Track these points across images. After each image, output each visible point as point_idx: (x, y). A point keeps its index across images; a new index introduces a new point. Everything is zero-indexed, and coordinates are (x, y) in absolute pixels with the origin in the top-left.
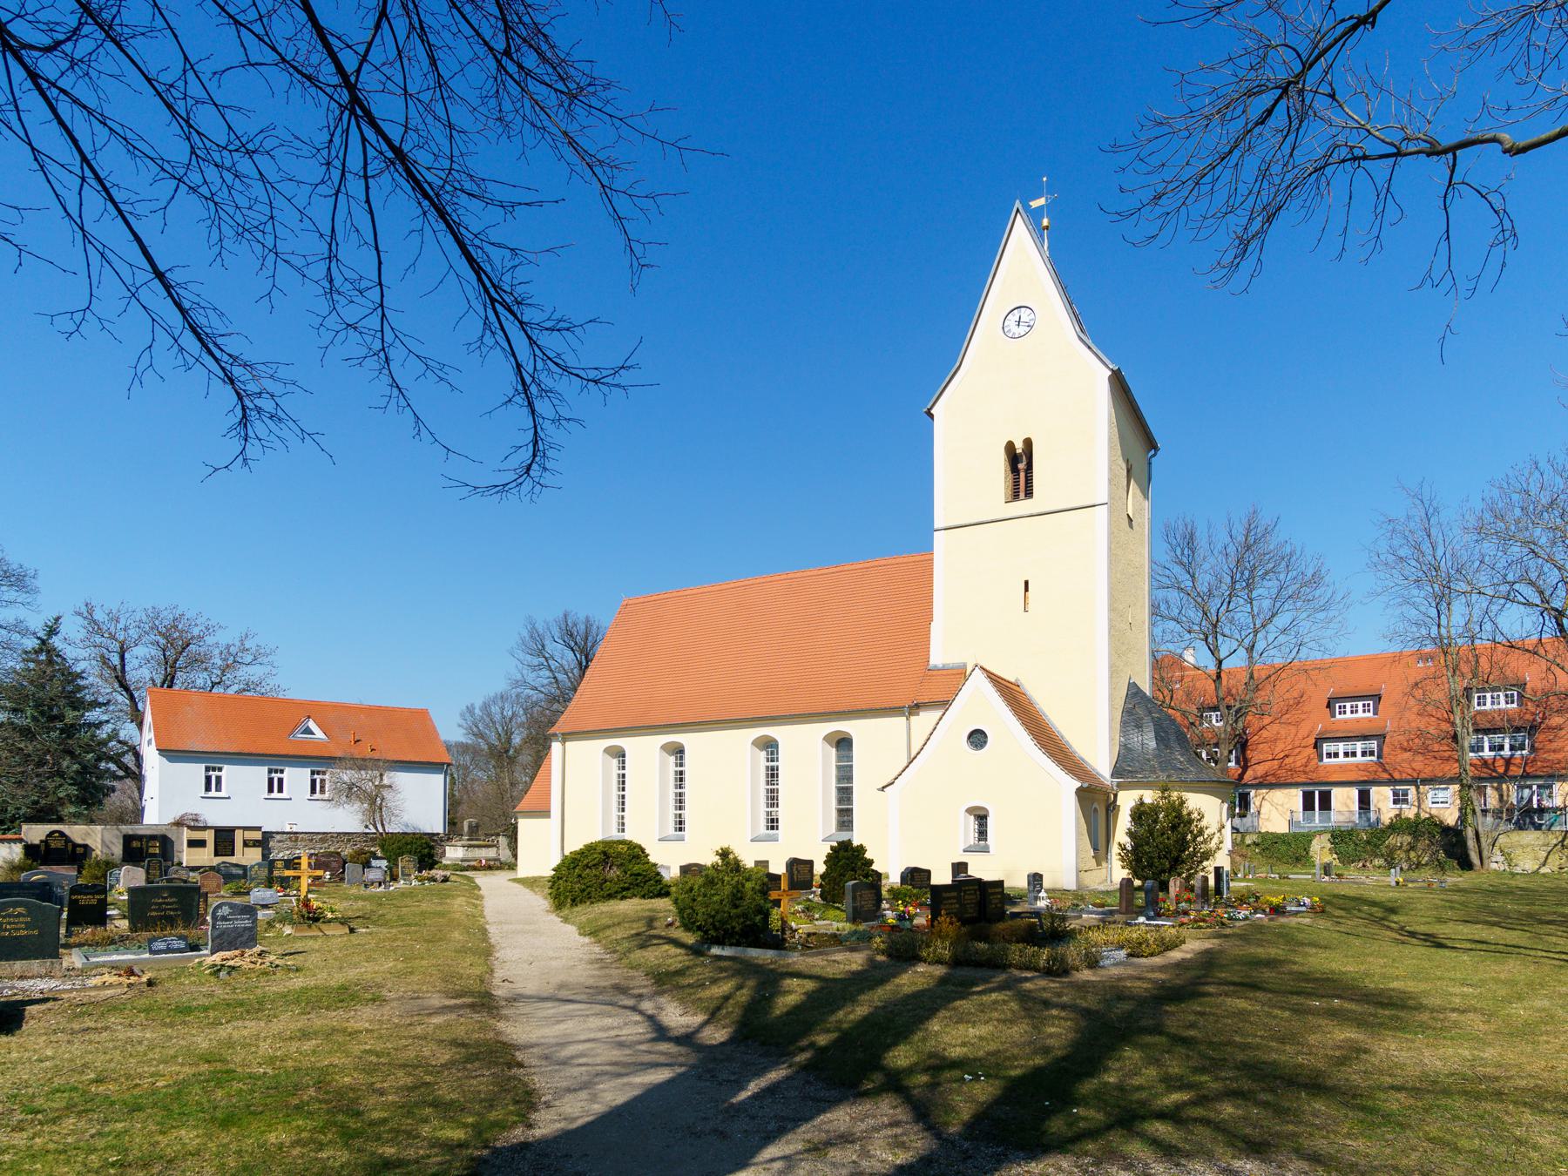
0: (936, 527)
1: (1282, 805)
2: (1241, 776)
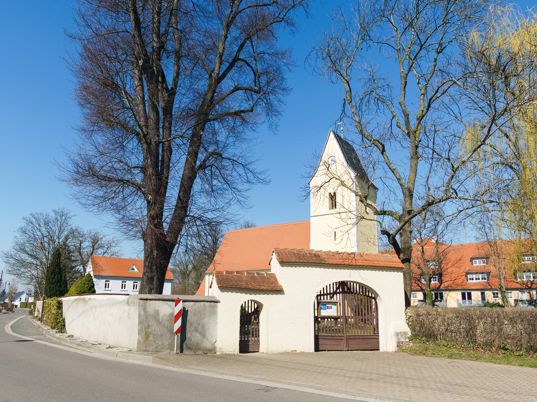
0: (311, 215)
2: (440, 286)
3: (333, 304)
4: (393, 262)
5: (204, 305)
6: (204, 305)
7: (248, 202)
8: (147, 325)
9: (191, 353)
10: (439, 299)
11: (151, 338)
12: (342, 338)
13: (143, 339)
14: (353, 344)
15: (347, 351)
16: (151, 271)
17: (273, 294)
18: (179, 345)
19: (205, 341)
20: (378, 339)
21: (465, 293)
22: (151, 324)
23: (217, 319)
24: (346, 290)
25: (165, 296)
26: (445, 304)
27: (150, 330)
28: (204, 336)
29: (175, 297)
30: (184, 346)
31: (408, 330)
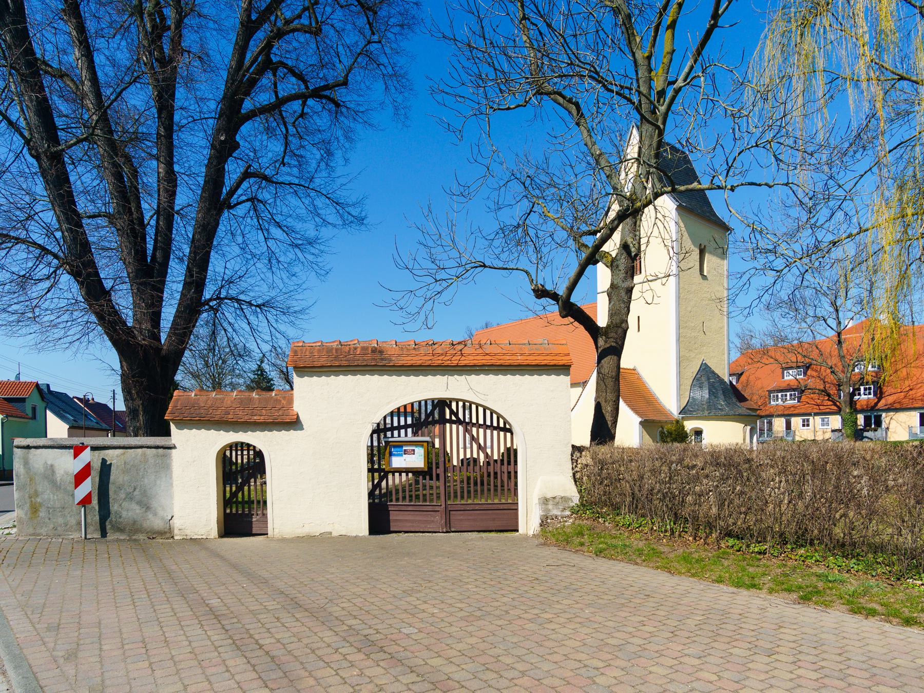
0: (598, 291)
1: (905, 423)
2: (876, 404)
3: (416, 446)
4: (539, 355)
5: (144, 455)
6: (144, 455)
7: (324, 264)
8: (32, 491)
9: (122, 538)
10: (873, 426)
11: (42, 514)
12: (437, 508)
13: (26, 514)
14: (461, 520)
15: (447, 532)
16: (133, 400)
17: (209, 429)
18: (98, 524)
19: (150, 516)
20: (517, 509)
21: (870, 417)
22: (40, 489)
23: (171, 478)
24: (448, 417)
25: (51, 439)
26: (884, 435)
27: (39, 500)
28: (148, 508)
29: (76, 441)
30: (108, 527)
31: (572, 492)
